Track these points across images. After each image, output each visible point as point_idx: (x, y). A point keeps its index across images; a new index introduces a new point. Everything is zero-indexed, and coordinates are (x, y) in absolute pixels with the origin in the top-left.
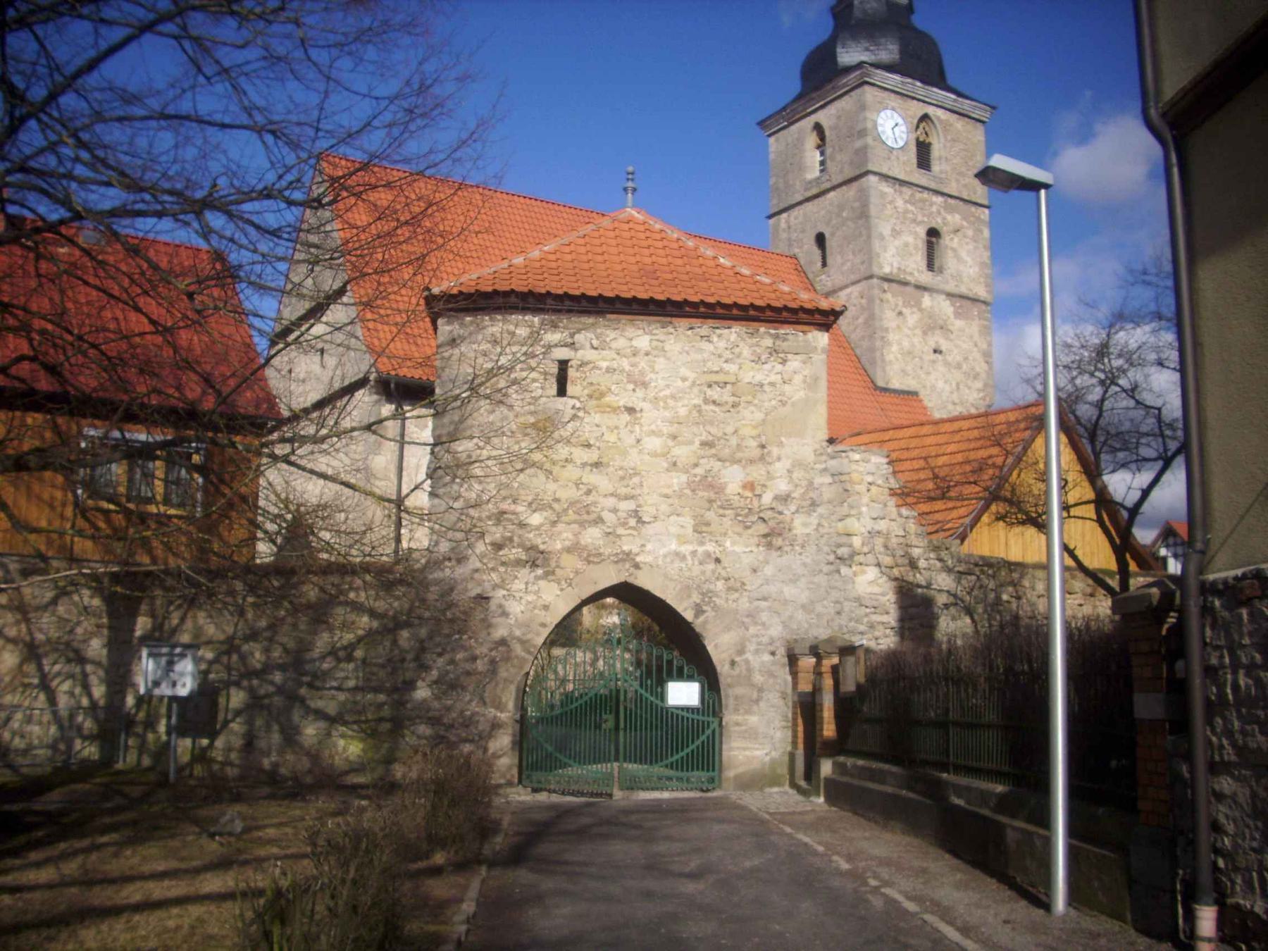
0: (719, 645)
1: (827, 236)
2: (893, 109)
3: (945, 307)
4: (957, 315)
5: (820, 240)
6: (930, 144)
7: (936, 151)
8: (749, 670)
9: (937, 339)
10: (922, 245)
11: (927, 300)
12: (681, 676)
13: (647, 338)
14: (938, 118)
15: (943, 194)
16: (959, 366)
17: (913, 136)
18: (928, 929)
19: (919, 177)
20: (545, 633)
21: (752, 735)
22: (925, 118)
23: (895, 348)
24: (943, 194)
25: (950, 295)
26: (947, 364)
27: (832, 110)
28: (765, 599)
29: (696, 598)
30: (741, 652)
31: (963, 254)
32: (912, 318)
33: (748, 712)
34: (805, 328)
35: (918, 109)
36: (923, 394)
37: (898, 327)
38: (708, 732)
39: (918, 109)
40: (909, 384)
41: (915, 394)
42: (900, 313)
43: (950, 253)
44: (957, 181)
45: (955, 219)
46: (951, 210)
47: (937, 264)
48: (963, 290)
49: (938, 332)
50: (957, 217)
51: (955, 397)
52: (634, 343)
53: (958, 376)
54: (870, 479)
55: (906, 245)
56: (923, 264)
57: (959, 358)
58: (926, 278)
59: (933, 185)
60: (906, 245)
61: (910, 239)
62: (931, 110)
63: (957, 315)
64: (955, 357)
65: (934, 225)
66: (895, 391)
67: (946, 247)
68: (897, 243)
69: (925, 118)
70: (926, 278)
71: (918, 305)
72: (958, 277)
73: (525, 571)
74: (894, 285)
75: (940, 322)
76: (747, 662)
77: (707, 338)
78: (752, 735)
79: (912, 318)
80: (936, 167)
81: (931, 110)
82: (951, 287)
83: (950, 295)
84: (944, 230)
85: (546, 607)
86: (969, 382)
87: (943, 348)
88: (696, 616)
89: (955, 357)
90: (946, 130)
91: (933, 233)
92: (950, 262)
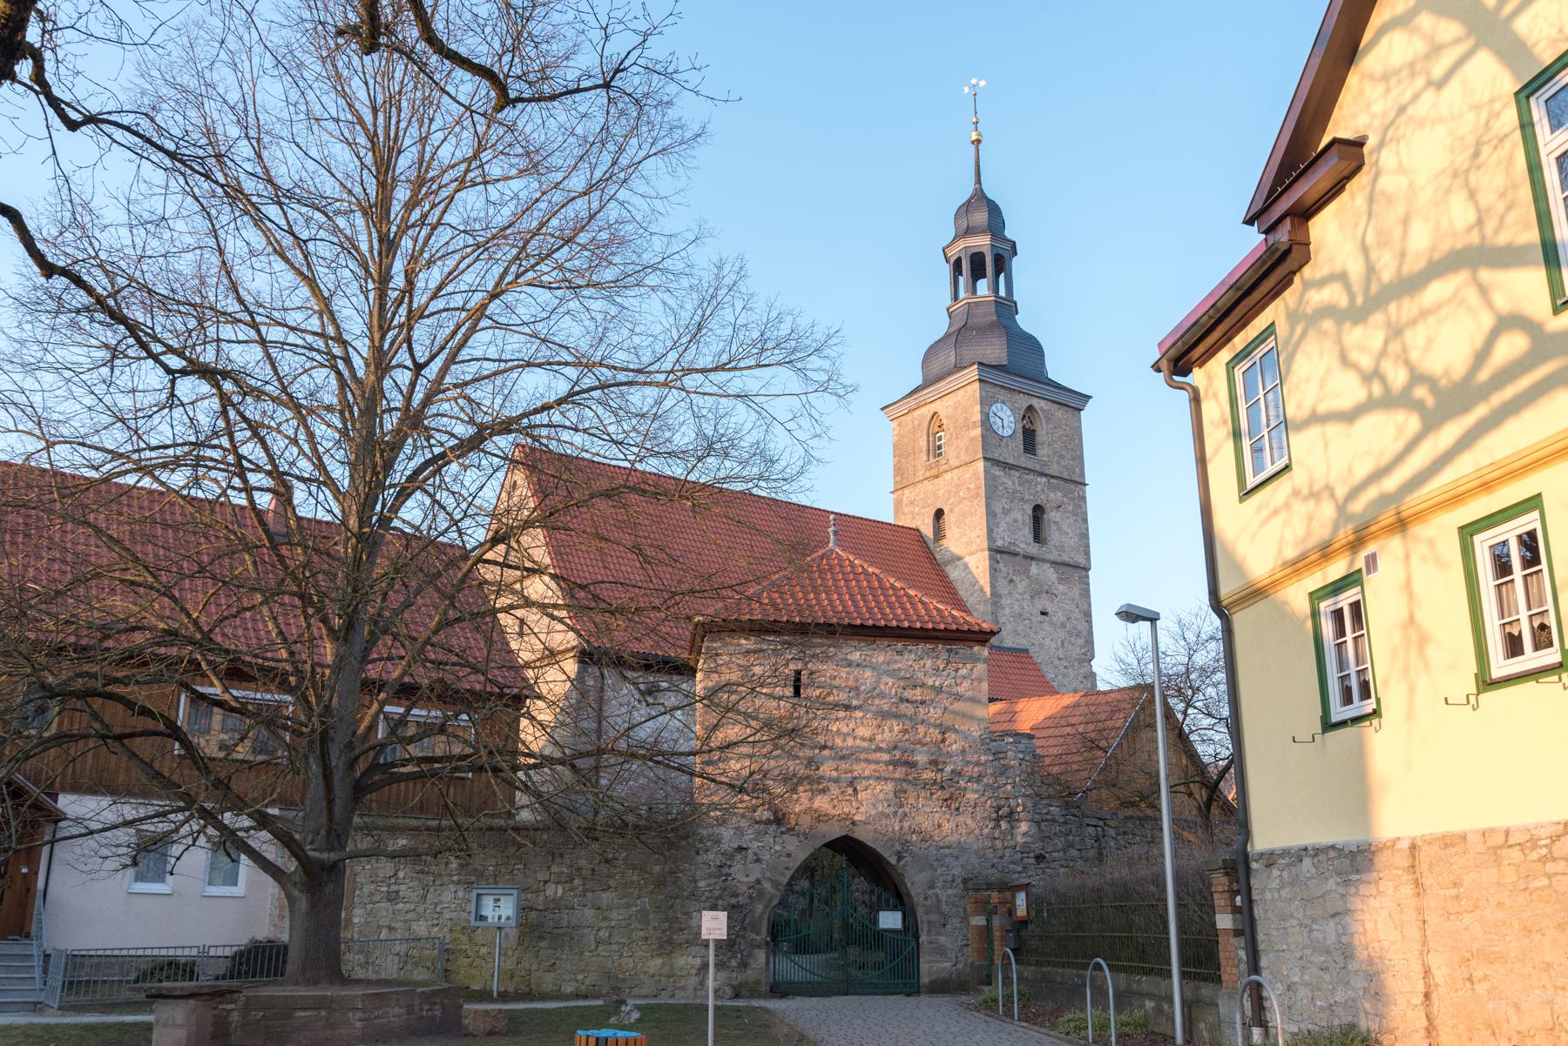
0: (915, 882)
1: (946, 511)
2: (1003, 402)
3: (1050, 574)
4: (1061, 580)
5: (939, 514)
6: (1034, 431)
7: (1042, 434)
8: (939, 901)
9: (1044, 603)
10: (1029, 521)
11: (1034, 569)
12: (888, 909)
13: (858, 653)
14: (1041, 408)
15: (1046, 475)
16: (1063, 625)
17: (1020, 426)
18: (1158, 833)
19: (1025, 461)
20: (789, 874)
21: (941, 951)
22: (1030, 408)
23: (1007, 611)
24: (1046, 475)
25: (1054, 563)
26: (1051, 623)
27: (949, 401)
28: (949, 847)
29: (898, 847)
30: (932, 887)
31: (1065, 527)
32: (1022, 584)
33: (939, 934)
34: (971, 644)
35: (1023, 402)
36: (1032, 650)
37: (1010, 593)
38: (909, 949)
39: (1023, 402)
40: (1022, 643)
41: (1027, 651)
42: (1011, 581)
43: (1054, 527)
44: (1059, 463)
45: (1055, 497)
46: (1051, 487)
47: (1042, 536)
48: (1065, 558)
49: (1044, 596)
50: (1059, 494)
51: (1061, 653)
52: (849, 657)
53: (1062, 634)
54: (1021, 756)
55: (1015, 521)
56: (1031, 537)
57: (1063, 619)
58: (1033, 549)
59: (1038, 468)
60: (1015, 521)
61: (1019, 516)
62: (1035, 402)
63: (1061, 580)
64: (1059, 617)
65: (1039, 502)
66: (1009, 649)
67: (1050, 521)
68: (1007, 519)
69: (1030, 408)
70: (1033, 549)
71: (1026, 572)
72: (1061, 549)
73: (774, 827)
74: (1005, 556)
75: (1046, 587)
76: (937, 895)
77: (899, 653)
78: (941, 951)
79: (1022, 584)
80: (1043, 451)
81: (1035, 402)
82: (1054, 556)
83: (1054, 563)
84: (1048, 507)
85: (789, 855)
86: (1072, 640)
87: (1049, 610)
88: (899, 861)
89: (1059, 617)
90: (1048, 420)
91: (1038, 511)
92: (1053, 535)
